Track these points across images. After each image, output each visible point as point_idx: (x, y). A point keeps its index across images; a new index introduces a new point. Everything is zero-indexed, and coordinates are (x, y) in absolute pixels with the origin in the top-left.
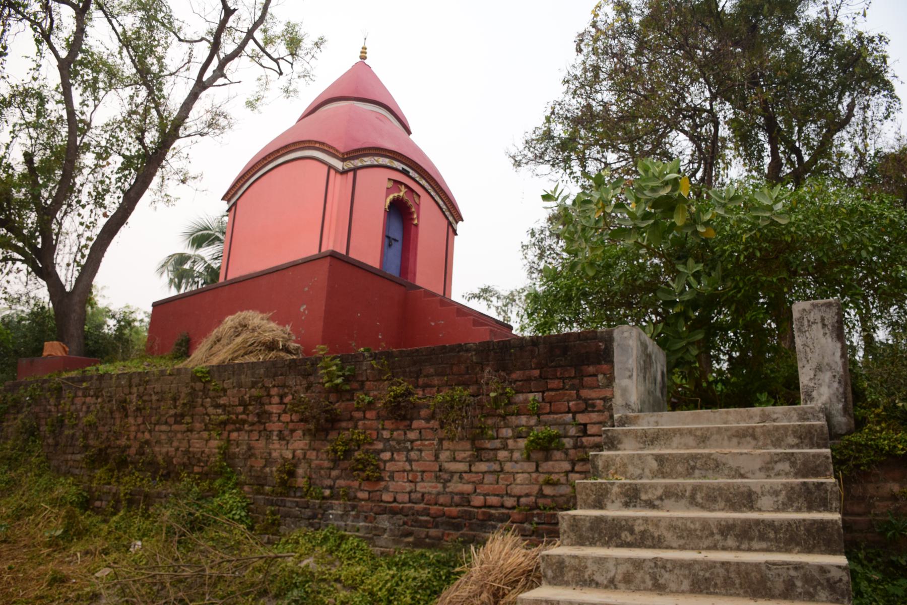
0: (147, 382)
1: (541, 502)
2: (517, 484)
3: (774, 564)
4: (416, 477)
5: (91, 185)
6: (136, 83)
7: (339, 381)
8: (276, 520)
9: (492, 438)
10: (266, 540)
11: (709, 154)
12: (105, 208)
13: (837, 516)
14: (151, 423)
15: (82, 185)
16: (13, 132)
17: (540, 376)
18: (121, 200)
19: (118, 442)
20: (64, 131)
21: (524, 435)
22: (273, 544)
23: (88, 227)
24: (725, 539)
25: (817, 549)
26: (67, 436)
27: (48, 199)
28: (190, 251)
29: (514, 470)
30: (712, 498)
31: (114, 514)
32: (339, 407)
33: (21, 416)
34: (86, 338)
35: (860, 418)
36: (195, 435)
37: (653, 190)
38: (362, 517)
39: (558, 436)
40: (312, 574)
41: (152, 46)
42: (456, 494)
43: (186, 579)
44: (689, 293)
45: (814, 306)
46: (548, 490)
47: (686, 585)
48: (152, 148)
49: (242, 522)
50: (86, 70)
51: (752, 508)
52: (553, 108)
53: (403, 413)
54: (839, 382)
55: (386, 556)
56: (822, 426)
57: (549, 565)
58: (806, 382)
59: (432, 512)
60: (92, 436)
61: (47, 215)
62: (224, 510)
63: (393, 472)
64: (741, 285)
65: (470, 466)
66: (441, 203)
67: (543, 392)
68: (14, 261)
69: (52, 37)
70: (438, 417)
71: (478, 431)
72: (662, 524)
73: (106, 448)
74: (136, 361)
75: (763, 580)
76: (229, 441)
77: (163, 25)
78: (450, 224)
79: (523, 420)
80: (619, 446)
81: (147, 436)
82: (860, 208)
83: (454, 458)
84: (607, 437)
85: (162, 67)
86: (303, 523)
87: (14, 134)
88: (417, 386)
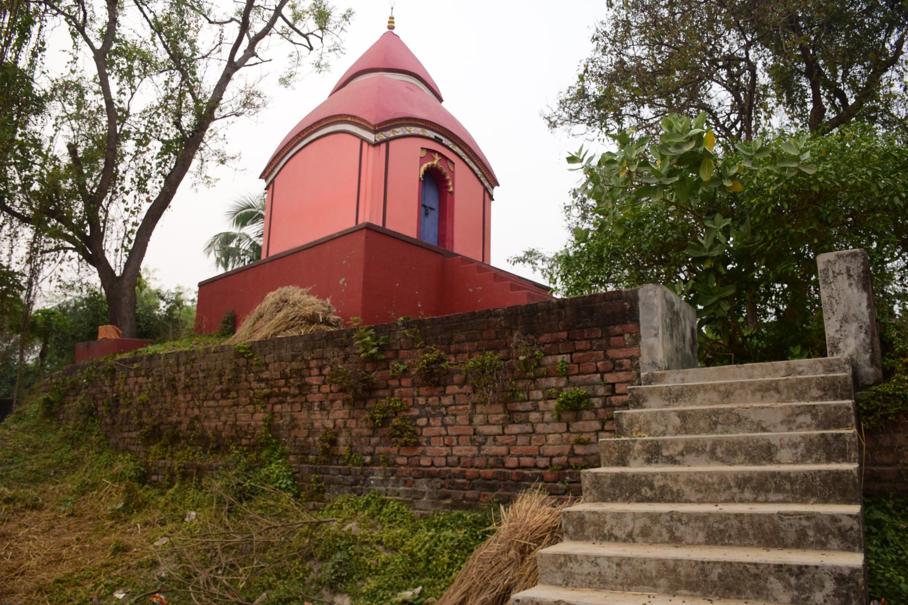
0: (193, 360)
1: (573, 461)
2: (549, 445)
3: (787, 514)
4: (452, 441)
5: (133, 172)
6: (170, 68)
7: (374, 351)
8: (320, 487)
9: (524, 401)
10: (311, 506)
11: (748, 103)
12: (148, 193)
13: (853, 467)
14: (199, 400)
15: (124, 172)
16: (56, 125)
17: (568, 338)
18: (162, 185)
19: (170, 419)
20: (104, 120)
21: (554, 396)
22: (318, 510)
23: (133, 213)
24: (743, 492)
25: (832, 499)
26: (123, 415)
27: (93, 188)
28: (235, 230)
29: (546, 431)
30: (731, 452)
31: (170, 487)
32: (376, 376)
33: (80, 398)
34: (137, 320)
35: (888, 368)
36: (241, 409)
37: (678, 146)
38: (401, 482)
39: (587, 397)
40: (354, 537)
41: (184, 30)
42: (491, 456)
43: (238, 545)
44: (710, 247)
45: (839, 256)
46: (579, 450)
47: (701, 537)
48: (189, 132)
49: (289, 490)
50: (122, 59)
51: (771, 461)
52: (586, 66)
53: (437, 379)
54: (866, 333)
55: (425, 518)
56: (846, 378)
57: (570, 521)
58: (832, 334)
59: (468, 474)
60: (145, 413)
61: (93, 202)
62: (272, 480)
63: (429, 437)
64: (770, 238)
65: (503, 428)
66: (475, 168)
67: (571, 354)
68: (66, 249)
69: (86, 29)
70: (470, 382)
71: (509, 394)
72: (681, 479)
73: (159, 425)
74: (185, 340)
75: (776, 530)
76: (273, 413)
77: (193, 8)
78: (486, 189)
79: (553, 381)
80: (644, 404)
81: (196, 411)
82: (894, 153)
83: (488, 421)
84: (633, 395)
85: (194, 50)
86: (346, 489)
87: (57, 127)
88: (449, 353)
